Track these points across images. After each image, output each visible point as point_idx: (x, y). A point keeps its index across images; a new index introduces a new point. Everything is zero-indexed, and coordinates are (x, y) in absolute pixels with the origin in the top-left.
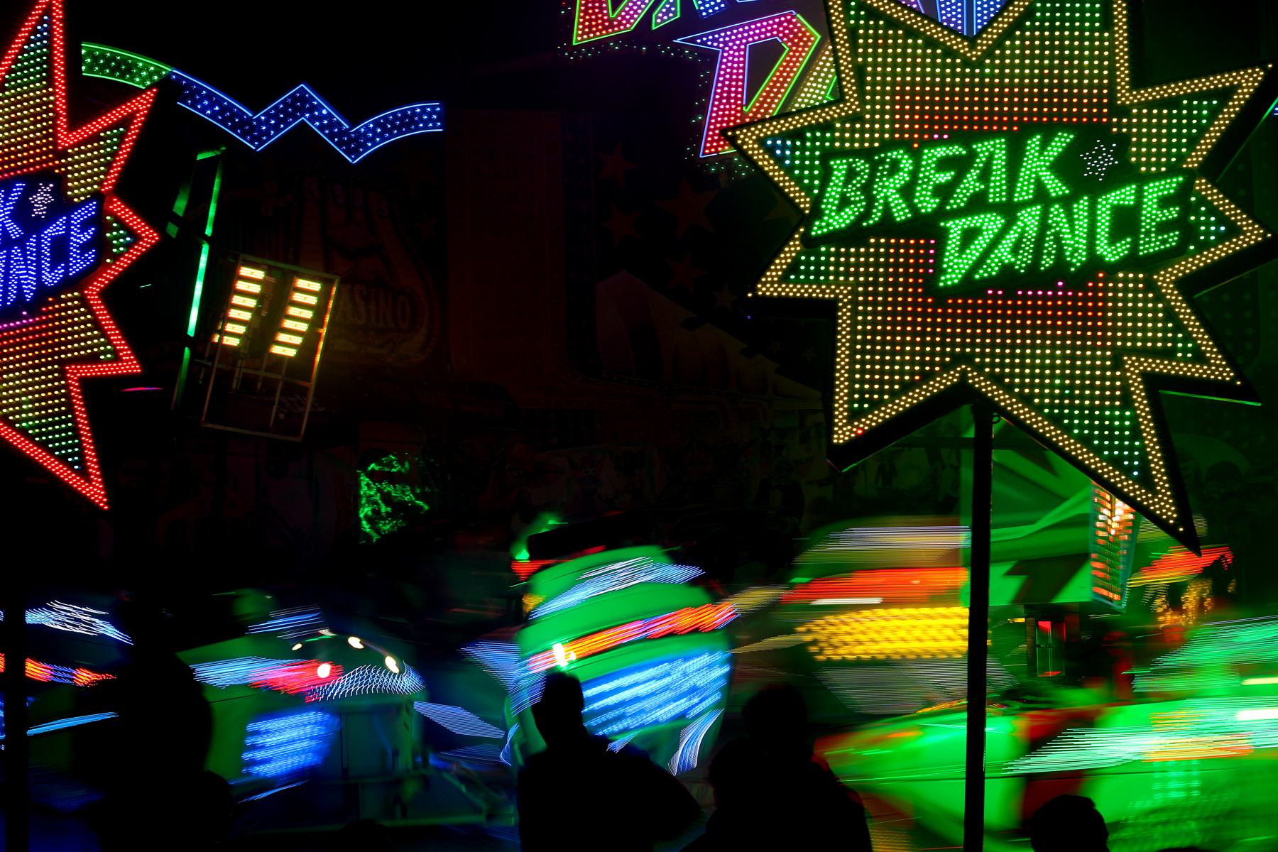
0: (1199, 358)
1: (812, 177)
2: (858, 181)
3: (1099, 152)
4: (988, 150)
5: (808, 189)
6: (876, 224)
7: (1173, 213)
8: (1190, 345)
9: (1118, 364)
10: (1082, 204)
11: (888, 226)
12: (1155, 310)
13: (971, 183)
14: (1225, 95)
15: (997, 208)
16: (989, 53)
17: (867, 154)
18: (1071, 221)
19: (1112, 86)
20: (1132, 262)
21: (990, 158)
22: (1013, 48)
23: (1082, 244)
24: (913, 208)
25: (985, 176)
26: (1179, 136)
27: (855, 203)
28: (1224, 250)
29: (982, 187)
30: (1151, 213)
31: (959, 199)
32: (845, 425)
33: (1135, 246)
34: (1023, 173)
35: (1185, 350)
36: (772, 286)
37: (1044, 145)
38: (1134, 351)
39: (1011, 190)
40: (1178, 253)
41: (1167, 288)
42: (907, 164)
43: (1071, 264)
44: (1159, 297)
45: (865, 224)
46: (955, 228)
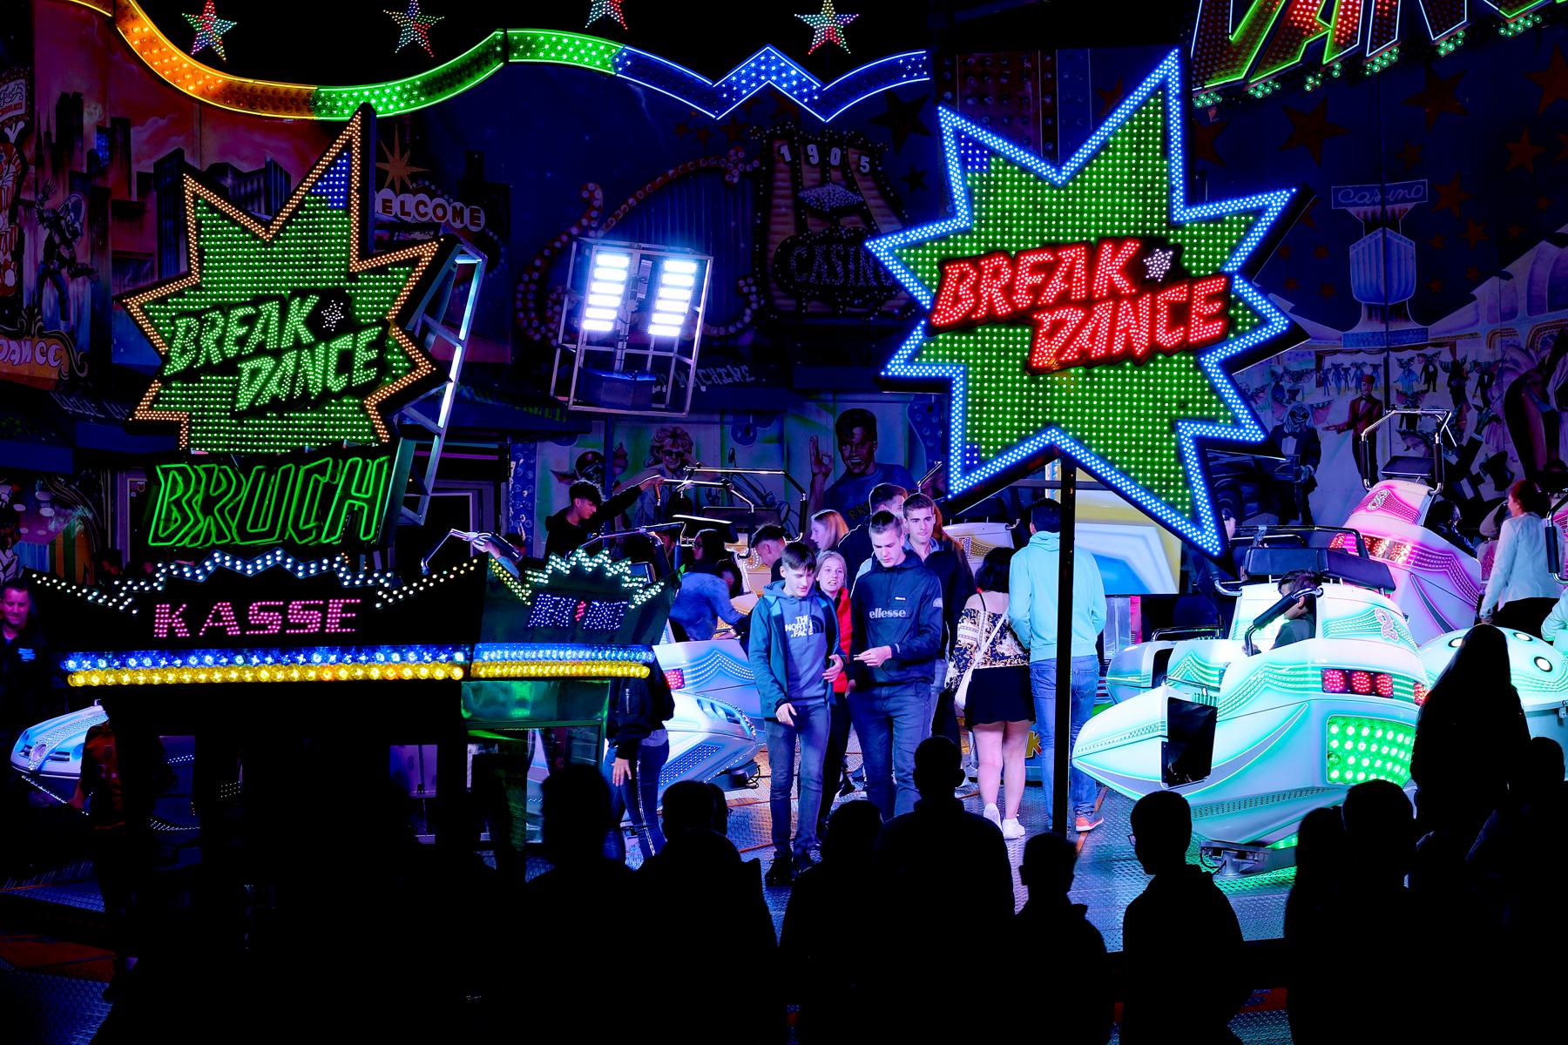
0: (1236, 423)
1: (931, 279)
2: (193, 335)
3: (333, 309)
4: (1071, 257)
5: (929, 288)
6: (202, 366)
7: (373, 354)
8: (1229, 414)
9: (1173, 427)
10: (321, 347)
11: (209, 368)
12: (1202, 386)
13: (1057, 285)
14: (1259, 212)
15: (1077, 304)
16: (1072, 178)
17: (197, 315)
18: (314, 361)
19: (1170, 206)
20: (348, 391)
21: (1073, 264)
22: (1091, 174)
23: (1144, 334)
24: (223, 354)
25: (1068, 278)
26: (1222, 246)
27: (190, 351)
28: (407, 380)
29: (1237, 277)
30: (362, 356)
31: (1050, 295)
32: (958, 479)
33: (349, 382)
34: (288, 326)
35: (1226, 418)
36: (951, 368)
37: (302, 304)
38: (1186, 419)
39: (280, 340)
40: (1221, 340)
41: (1212, 368)
42: (220, 322)
43: (312, 394)
44: (1206, 375)
45: (923, 322)
46: (246, 367)
